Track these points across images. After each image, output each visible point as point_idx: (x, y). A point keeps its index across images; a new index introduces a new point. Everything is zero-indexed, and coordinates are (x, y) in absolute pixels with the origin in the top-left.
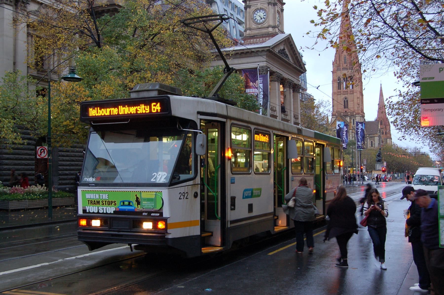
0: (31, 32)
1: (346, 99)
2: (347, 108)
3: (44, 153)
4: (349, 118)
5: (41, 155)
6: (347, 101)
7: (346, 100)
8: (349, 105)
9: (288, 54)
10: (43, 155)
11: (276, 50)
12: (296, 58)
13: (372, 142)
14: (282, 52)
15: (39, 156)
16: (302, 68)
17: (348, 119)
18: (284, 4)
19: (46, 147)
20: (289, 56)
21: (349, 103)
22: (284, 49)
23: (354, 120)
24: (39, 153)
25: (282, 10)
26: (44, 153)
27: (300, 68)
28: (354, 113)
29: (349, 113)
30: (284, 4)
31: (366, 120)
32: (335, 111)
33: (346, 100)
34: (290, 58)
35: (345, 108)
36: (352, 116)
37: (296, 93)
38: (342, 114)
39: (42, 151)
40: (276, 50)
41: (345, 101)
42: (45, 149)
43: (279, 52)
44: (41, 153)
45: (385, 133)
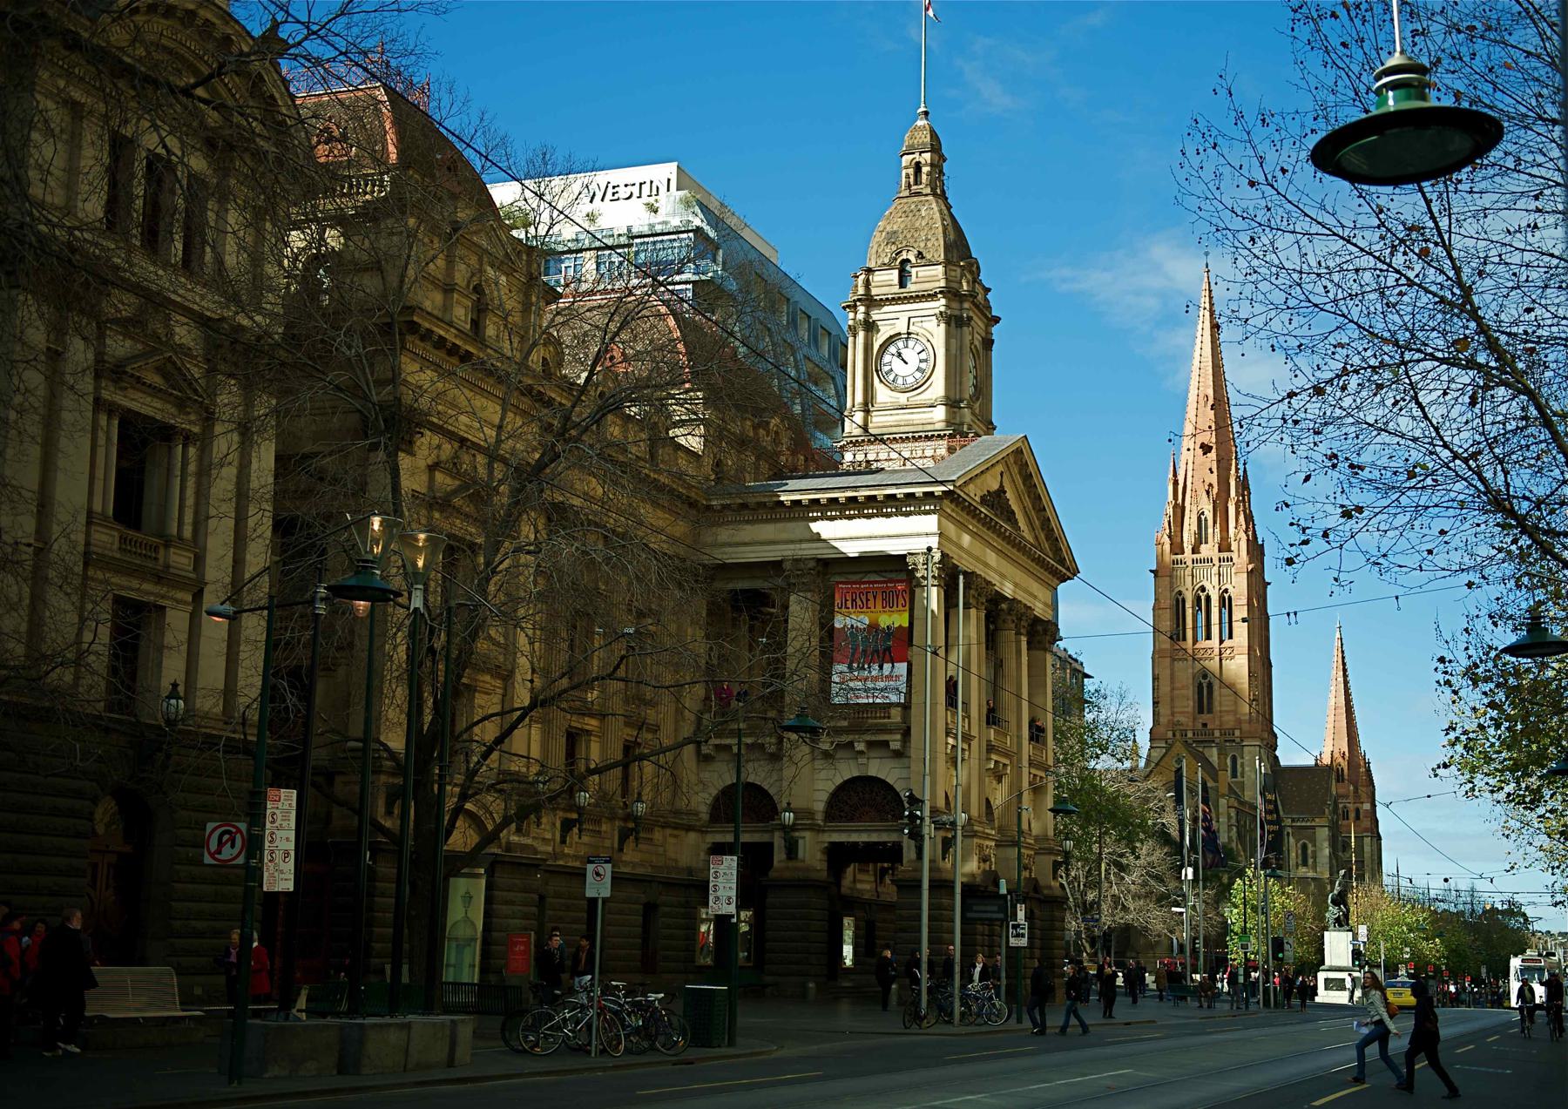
0: (105, 395)
1: (1205, 677)
2: (1210, 711)
3: (233, 846)
4: (1215, 751)
5: (219, 852)
6: (1210, 685)
7: (1203, 596)
8: (1216, 704)
9: (1015, 507)
10: (227, 853)
11: (974, 493)
12: (1042, 525)
13: (1304, 847)
14: (996, 499)
15: (212, 855)
16: (1062, 562)
17: (1213, 755)
18: (997, 320)
19: (243, 826)
20: (1020, 516)
21: (1216, 693)
22: (1002, 491)
23: (1234, 759)
24: (213, 846)
25: (988, 343)
26: (233, 846)
27: (1057, 565)
28: (1237, 733)
29: (1217, 733)
30: (997, 320)
31: (1283, 763)
32: (1163, 720)
33: (1203, 596)
34: (1022, 524)
35: (1201, 711)
36: (1230, 742)
37: (1039, 653)
38: (1190, 734)
39: (226, 837)
40: (974, 493)
41: (1200, 686)
42: (239, 831)
43: (983, 500)
44: (221, 844)
45: (1352, 815)
